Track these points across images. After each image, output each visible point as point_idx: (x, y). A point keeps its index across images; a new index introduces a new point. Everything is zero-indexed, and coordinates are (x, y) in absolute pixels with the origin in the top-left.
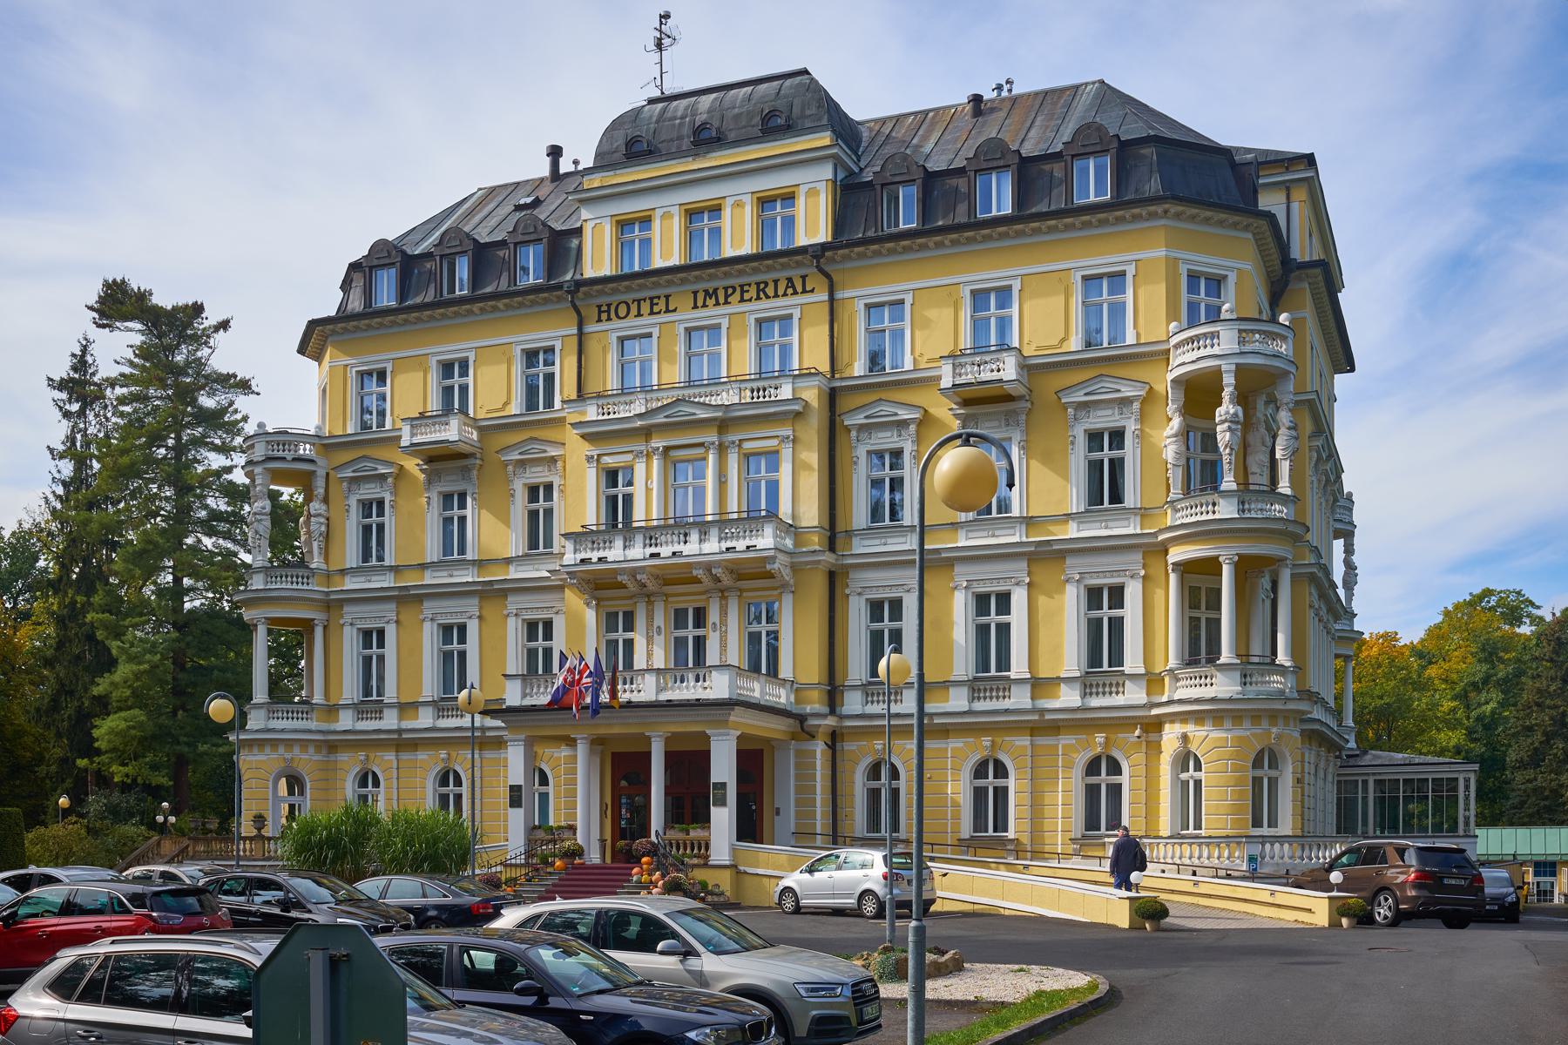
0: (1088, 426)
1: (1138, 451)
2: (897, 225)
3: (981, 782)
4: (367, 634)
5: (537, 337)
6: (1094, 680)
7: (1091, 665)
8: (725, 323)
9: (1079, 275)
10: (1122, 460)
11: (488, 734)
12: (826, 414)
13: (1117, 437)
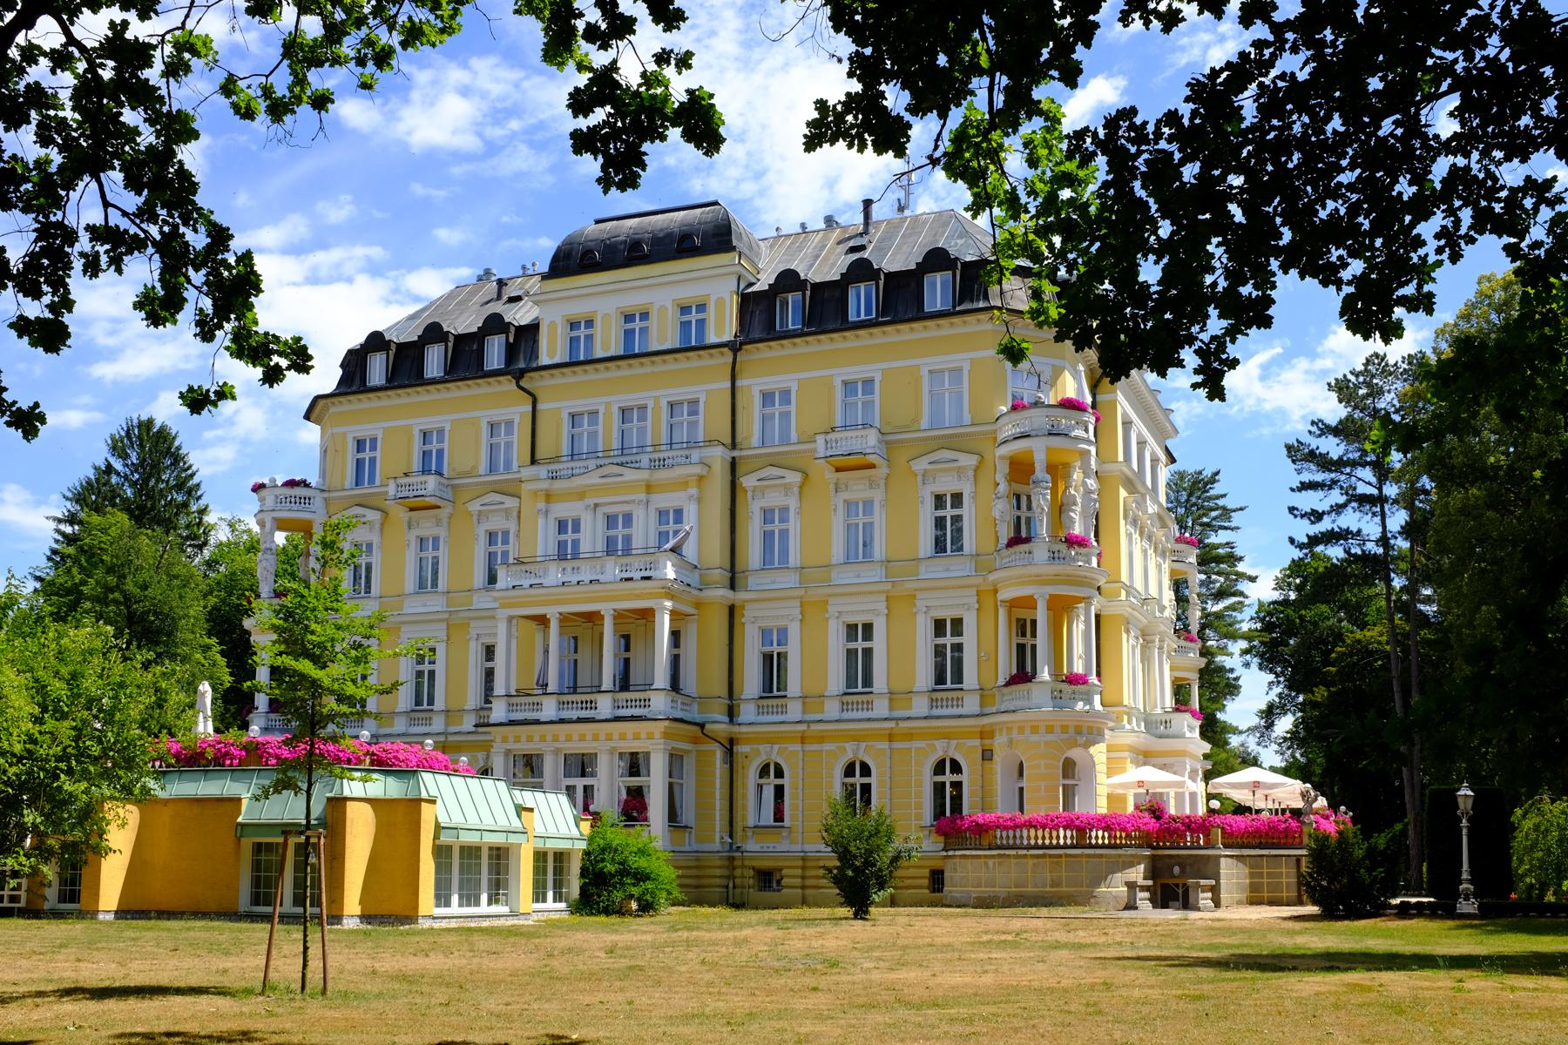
0: (763, 505)
1: (884, 516)
2: (859, 315)
3: (940, 779)
4: (851, 629)
5: (498, 414)
6: (939, 695)
7: (937, 683)
8: (966, 367)
9: (927, 369)
10: (871, 524)
11: (451, 738)
12: (728, 477)
13: (957, 499)
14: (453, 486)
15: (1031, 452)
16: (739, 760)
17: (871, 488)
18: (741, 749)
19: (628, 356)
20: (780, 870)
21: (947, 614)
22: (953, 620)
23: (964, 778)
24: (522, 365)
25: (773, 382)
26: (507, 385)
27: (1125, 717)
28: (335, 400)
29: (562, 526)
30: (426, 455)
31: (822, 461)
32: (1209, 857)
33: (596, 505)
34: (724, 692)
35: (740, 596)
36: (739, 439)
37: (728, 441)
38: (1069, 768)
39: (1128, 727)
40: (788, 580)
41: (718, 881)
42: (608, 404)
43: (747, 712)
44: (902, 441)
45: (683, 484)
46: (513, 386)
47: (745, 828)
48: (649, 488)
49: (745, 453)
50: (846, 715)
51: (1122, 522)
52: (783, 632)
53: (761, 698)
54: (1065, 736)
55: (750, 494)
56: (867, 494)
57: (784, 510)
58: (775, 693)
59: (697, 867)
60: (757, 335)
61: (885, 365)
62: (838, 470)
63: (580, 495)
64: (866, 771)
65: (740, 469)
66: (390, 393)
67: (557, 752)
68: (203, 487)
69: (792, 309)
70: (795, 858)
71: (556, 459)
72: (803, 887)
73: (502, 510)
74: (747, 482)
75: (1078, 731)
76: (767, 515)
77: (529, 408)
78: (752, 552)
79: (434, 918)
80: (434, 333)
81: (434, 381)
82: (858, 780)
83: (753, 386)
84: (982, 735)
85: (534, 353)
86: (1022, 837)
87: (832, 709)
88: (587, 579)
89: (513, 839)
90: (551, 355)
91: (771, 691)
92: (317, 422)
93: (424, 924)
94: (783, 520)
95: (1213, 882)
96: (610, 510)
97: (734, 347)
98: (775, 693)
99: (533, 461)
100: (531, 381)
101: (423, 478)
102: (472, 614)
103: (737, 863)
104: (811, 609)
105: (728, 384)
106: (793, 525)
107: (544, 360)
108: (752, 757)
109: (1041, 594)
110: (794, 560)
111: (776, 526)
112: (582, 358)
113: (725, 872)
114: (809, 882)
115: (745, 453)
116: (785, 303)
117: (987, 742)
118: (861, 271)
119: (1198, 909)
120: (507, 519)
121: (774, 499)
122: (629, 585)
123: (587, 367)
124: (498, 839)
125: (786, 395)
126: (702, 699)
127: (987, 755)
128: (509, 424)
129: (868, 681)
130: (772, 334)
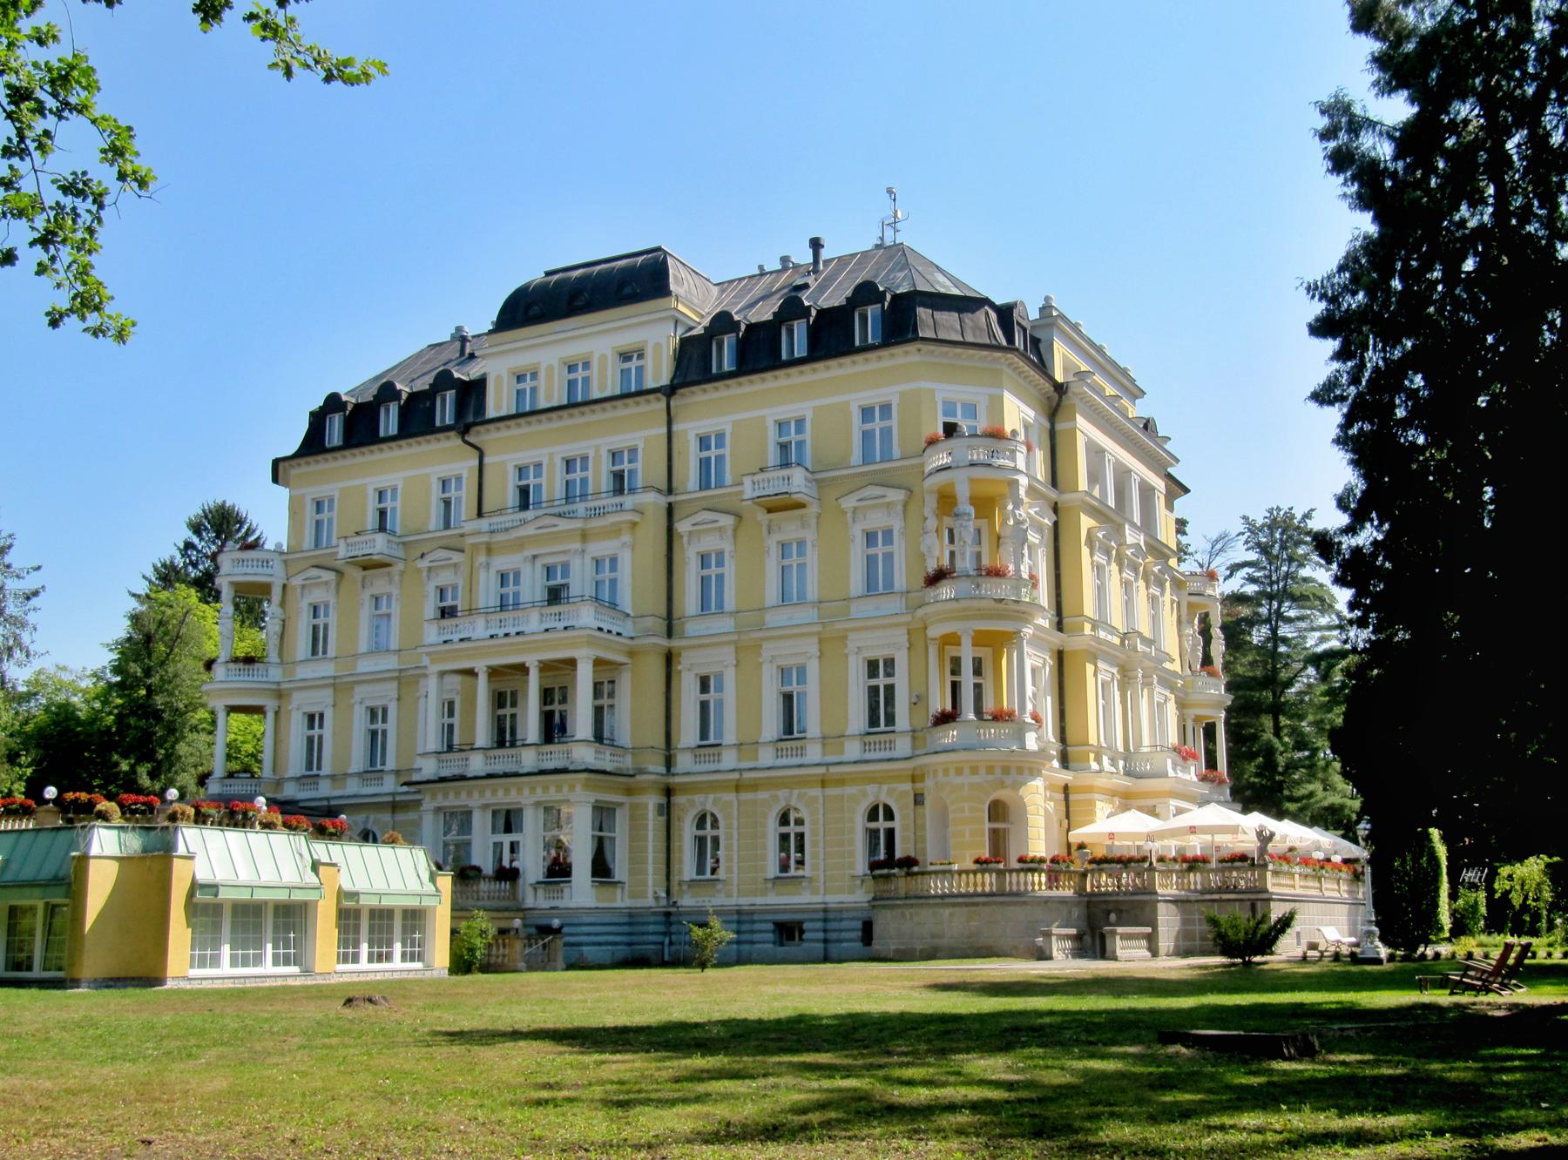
1: (903, 545)
3: (873, 825)
10: (804, 564)
14: (404, 544)
15: (952, 485)
16: (675, 813)
17: (803, 527)
18: (679, 800)
19: (572, 405)
20: (800, 923)
21: (879, 654)
22: (885, 662)
23: (896, 824)
24: (470, 419)
25: (708, 425)
26: (453, 441)
27: (1092, 756)
28: (294, 462)
29: (503, 578)
30: (784, 447)
31: (750, 502)
32: (1144, 902)
33: (535, 557)
34: (660, 741)
35: (675, 643)
36: (675, 484)
37: (664, 487)
38: (998, 811)
39: (1095, 766)
40: (725, 624)
41: (652, 938)
42: (551, 455)
43: (684, 762)
44: (833, 479)
45: (615, 531)
46: (459, 442)
47: (680, 883)
48: (584, 536)
49: (679, 498)
50: (868, 756)
51: (1085, 551)
52: (802, 671)
53: (781, 740)
54: (990, 777)
55: (685, 539)
56: (800, 534)
57: (720, 555)
58: (796, 735)
59: (630, 924)
60: (695, 377)
61: (818, 403)
62: (770, 511)
63: (519, 544)
64: (889, 815)
65: (677, 514)
66: (403, 443)
67: (485, 807)
68: (264, 535)
69: (725, 354)
70: (815, 911)
71: (501, 511)
72: (826, 941)
73: (450, 565)
74: (682, 527)
75: (1006, 770)
76: (704, 560)
77: (476, 462)
78: (689, 599)
79: (189, 979)
80: (387, 391)
81: (794, 363)
82: (882, 824)
83: (689, 429)
84: (914, 779)
85: (481, 407)
86: (1018, 883)
87: (853, 750)
88: (513, 631)
89: (426, 902)
90: (602, 391)
91: (791, 732)
92: (286, 485)
93: (170, 984)
94: (720, 563)
95: (1149, 930)
96: (550, 560)
97: (670, 391)
98: (796, 735)
99: (480, 514)
100: (479, 436)
101: (785, 472)
102: (355, 679)
103: (673, 919)
104: (746, 650)
105: (664, 430)
106: (729, 570)
107: (491, 413)
108: (687, 809)
109: (966, 629)
110: (730, 603)
111: (713, 571)
112: (580, 399)
113: (661, 928)
114: (832, 936)
115: (679, 498)
116: (864, 318)
117: (919, 785)
118: (792, 308)
119: (1115, 958)
120: (390, 582)
121: (710, 543)
122: (447, 647)
123: (586, 409)
124: (413, 903)
125: (886, 409)
126: (636, 750)
127: (919, 800)
128: (459, 479)
129: (890, 719)
130: (706, 376)
